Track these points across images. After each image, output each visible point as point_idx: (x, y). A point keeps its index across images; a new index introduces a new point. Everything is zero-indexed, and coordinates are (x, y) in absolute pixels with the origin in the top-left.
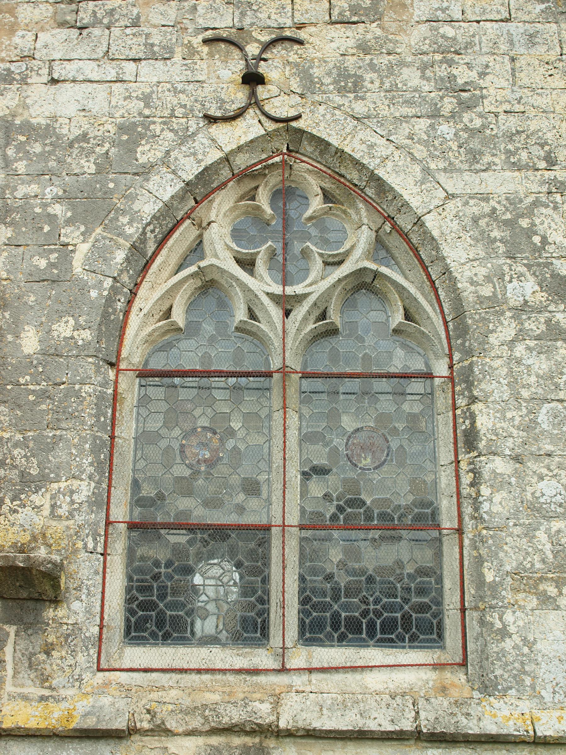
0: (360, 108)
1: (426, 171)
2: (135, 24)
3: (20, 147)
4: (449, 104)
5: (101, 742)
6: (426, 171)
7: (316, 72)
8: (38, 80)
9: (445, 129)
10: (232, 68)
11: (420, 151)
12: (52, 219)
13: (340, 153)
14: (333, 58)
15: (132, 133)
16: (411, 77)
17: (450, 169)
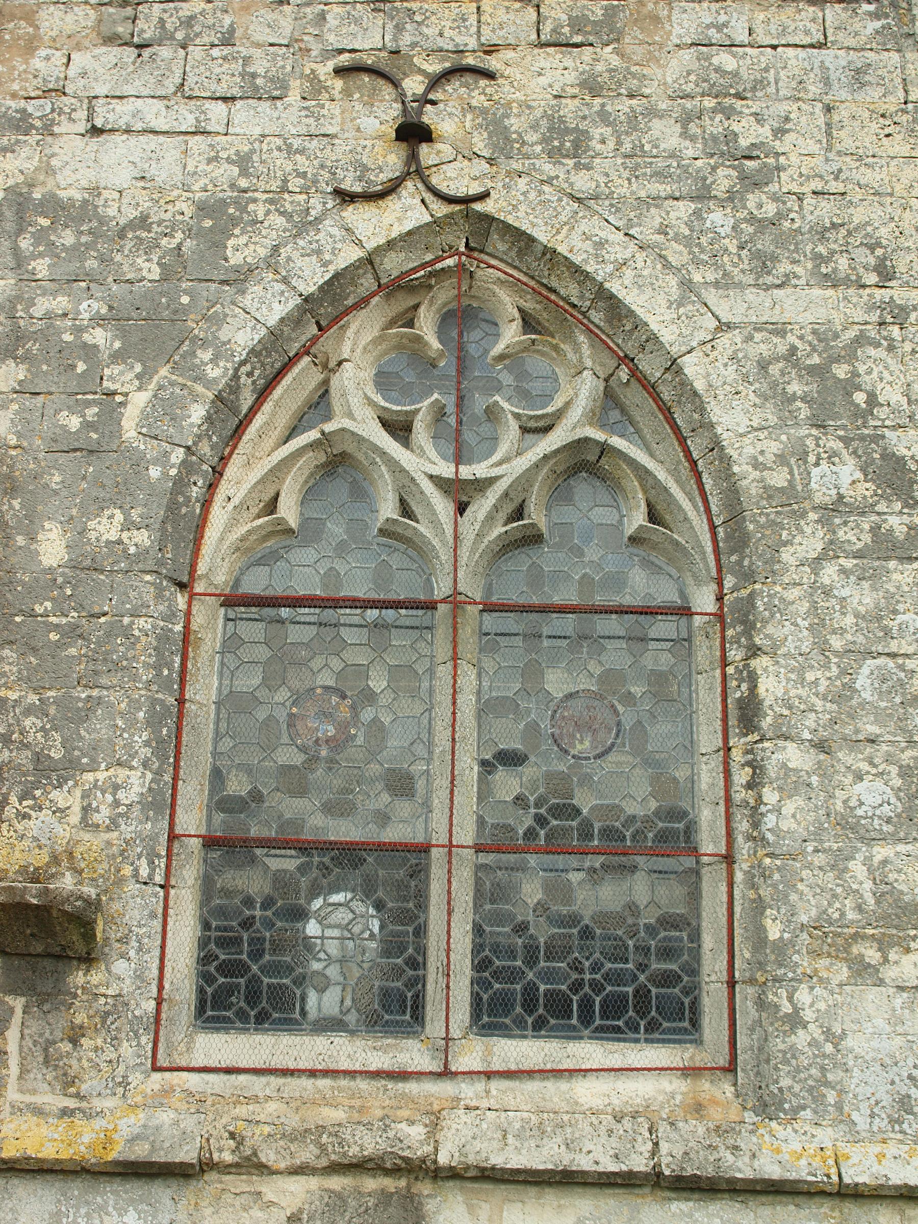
0: (583, 182)
1: (687, 285)
2: (227, 40)
3: (41, 236)
4: (724, 179)
5: (156, 1182)
6: (687, 285)
7: (514, 123)
8: (70, 128)
9: (719, 218)
10: (380, 116)
11: (677, 254)
12: (90, 351)
13: (549, 254)
14: (542, 102)
15: (220, 217)
16: (666, 134)
17: (725, 283)
